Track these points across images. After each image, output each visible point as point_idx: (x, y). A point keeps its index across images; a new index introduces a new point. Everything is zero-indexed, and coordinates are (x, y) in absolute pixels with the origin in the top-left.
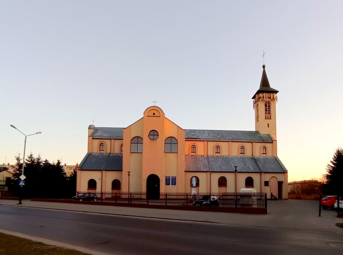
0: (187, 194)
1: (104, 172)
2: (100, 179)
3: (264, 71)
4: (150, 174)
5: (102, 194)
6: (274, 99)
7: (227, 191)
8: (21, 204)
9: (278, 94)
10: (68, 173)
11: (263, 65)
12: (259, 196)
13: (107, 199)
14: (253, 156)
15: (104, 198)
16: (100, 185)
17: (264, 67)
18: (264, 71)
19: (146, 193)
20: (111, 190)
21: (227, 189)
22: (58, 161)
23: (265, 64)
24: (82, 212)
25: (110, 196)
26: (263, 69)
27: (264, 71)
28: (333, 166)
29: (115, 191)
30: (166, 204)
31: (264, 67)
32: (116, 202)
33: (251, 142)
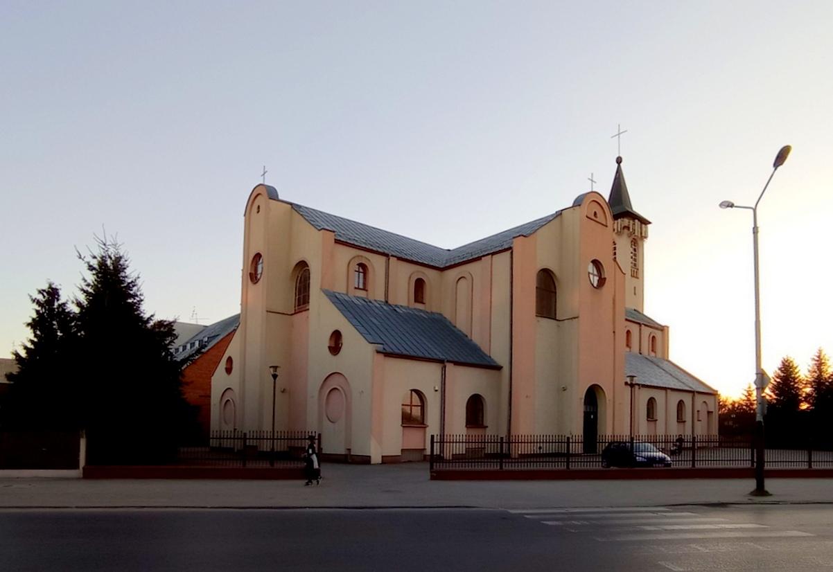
0: (568, 438)
1: (450, 367)
2: (436, 391)
3: (619, 172)
4: (589, 385)
5: (694, 441)
6: (643, 237)
7: (657, 431)
8: (765, 494)
9: (649, 226)
10: (179, 348)
11: (617, 156)
12: (662, 442)
13: (457, 458)
14: (641, 354)
15: (447, 455)
16: (691, 415)
17: (619, 161)
18: (617, 172)
19: (581, 439)
20: (465, 429)
21: (657, 428)
22: (820, 351)
23: (621, 155)
24: (77, 507)
25: (460, 449)
26: (617, 165)
27: (619, 172)
28: (32, 347)
29: (475, 432)
30: (693, 465)
31: (619, 161)
32: (244, 465)
33: (639, 324)
